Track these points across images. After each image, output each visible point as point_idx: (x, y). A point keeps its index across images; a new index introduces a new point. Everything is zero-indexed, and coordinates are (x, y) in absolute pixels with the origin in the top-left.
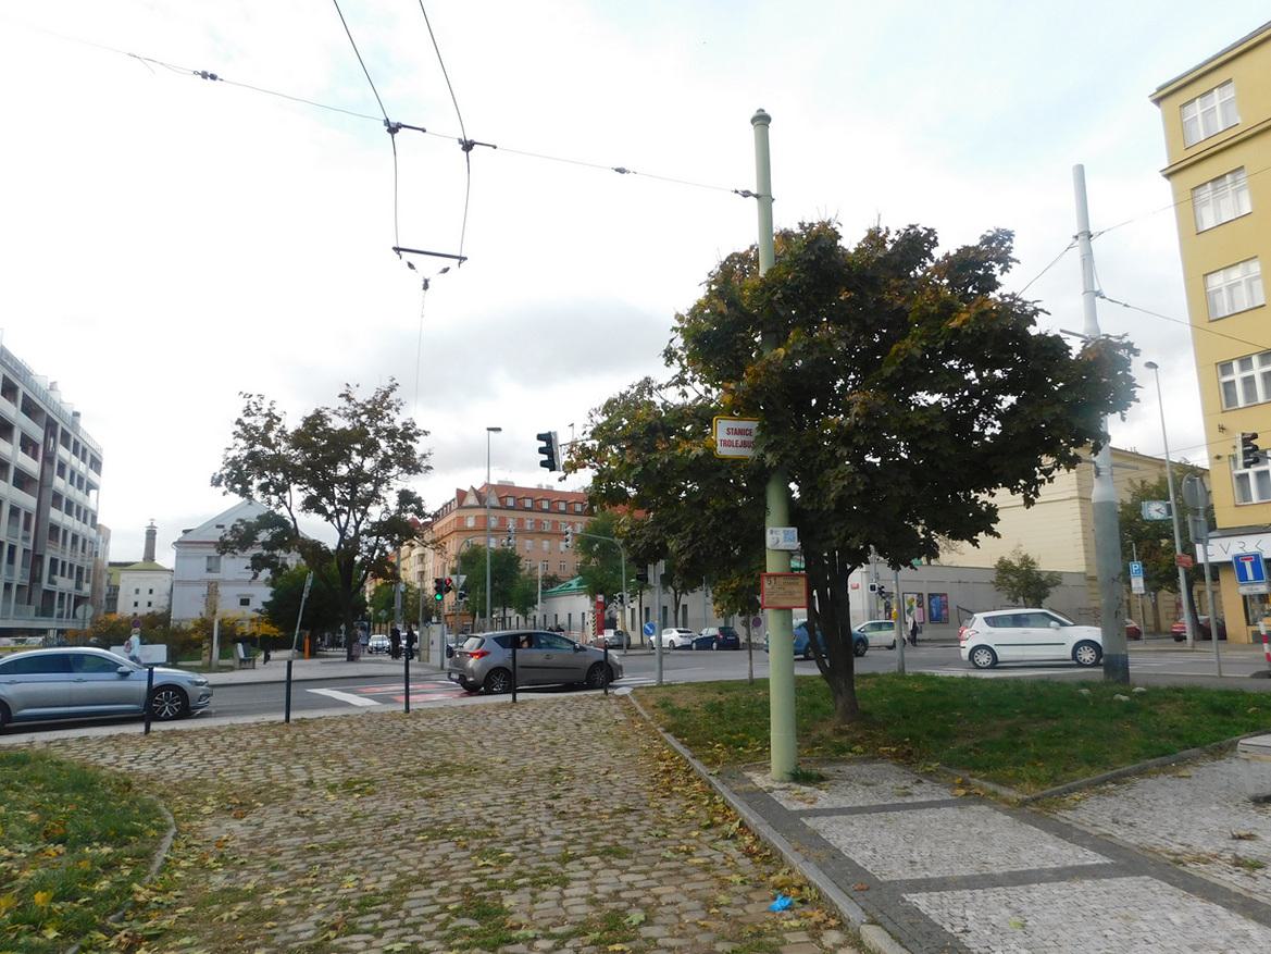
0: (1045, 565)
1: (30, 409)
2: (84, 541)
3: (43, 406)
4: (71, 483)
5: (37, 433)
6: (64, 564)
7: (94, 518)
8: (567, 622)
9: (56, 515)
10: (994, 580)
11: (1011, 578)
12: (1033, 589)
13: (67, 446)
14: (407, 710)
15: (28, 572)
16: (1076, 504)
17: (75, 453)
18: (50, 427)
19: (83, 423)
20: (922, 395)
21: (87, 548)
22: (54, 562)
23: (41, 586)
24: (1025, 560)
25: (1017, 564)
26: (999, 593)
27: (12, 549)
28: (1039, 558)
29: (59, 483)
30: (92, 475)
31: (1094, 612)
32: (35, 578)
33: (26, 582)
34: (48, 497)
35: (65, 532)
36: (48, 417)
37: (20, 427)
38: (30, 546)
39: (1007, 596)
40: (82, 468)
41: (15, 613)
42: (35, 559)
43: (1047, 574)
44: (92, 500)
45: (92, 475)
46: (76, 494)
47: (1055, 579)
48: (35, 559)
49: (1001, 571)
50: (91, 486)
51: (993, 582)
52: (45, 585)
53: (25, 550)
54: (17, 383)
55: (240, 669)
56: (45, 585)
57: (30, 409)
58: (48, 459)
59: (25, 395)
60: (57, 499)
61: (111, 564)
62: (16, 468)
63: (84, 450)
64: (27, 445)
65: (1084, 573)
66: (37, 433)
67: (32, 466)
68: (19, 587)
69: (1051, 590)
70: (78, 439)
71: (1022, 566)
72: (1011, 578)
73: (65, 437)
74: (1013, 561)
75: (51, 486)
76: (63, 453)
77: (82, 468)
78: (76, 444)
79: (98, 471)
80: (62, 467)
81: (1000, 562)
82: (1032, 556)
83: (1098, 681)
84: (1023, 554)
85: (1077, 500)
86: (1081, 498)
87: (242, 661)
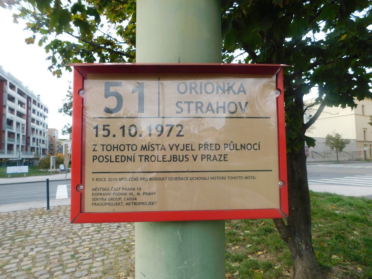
0: (344, 137)
1: (21, 93)
2: (44, 133)
3: (25, 92)
4: (38, 115)
5: (24, 100)
6: (37, 139)
7: (47, 126)
8: (338, 153)
9: (33, 125)
10: (325, 142)
11: (331, 141)
12: (339, 145)
13: (35, 105)
14: (48, 208)
15: (25, 142)
16: (354, 116)
17: (39, 106)
18: (29, 99)
19: (41, 98)
20: (356, 13)
21: (45, 135)
22: (34, 139)
23: (30, 146)
24: (338, 135)
25: (334, 136)
26: (327, 146)
27: (18, 135)
28: (342, 134)
29: (33, 116)
30: (45, 113)
31: (359, 153)
32: (28, 143)
33: (25, 145)
34: (30, 120)
35: (37, 130)
36: (28, 96)
37: (17, 98)
38: (25, 134)
39: (330, 147)
40: (42, 111)
41: (7, 153)
42: (27, 138)
43: (344, 140)
44: (46, 121)
45: (45, 113)
46: (41, 119)
47: (348, 142)
48: (27, 138)
49: (328, 139)
50: (45, 117)
51: (325, 143)
52: (31, 145)
53: (23, 136)
54: (15, 85)
55: (61, 173)
56: (31, 145)
57: (21, 93)
58: (29, 108)
59: (18, 89)
60: (33, 120)
61: (59, 140)
62: (17, 111)
63: (42, 106)
64: (21, 103)
65: (356, 140)
66: (24, 100)
67: (24, 111)
68: (22, 146)
69: (346, 145)
70: (39, 103)
71: (336, 137)
72: (331, 141)
73: (35, 102)
74: (332, 135)
75: (31, 116)
76: (34, 107)
77: (42, 111)
78: (39, 104)
79: (47, 112)
80: (34, 111)
81: (327, 136)
82: (339, 134)
83: (107, 132)
84: (337, 133)
85: (354, 115)
86: (355, 114)
87: (62, 171)
